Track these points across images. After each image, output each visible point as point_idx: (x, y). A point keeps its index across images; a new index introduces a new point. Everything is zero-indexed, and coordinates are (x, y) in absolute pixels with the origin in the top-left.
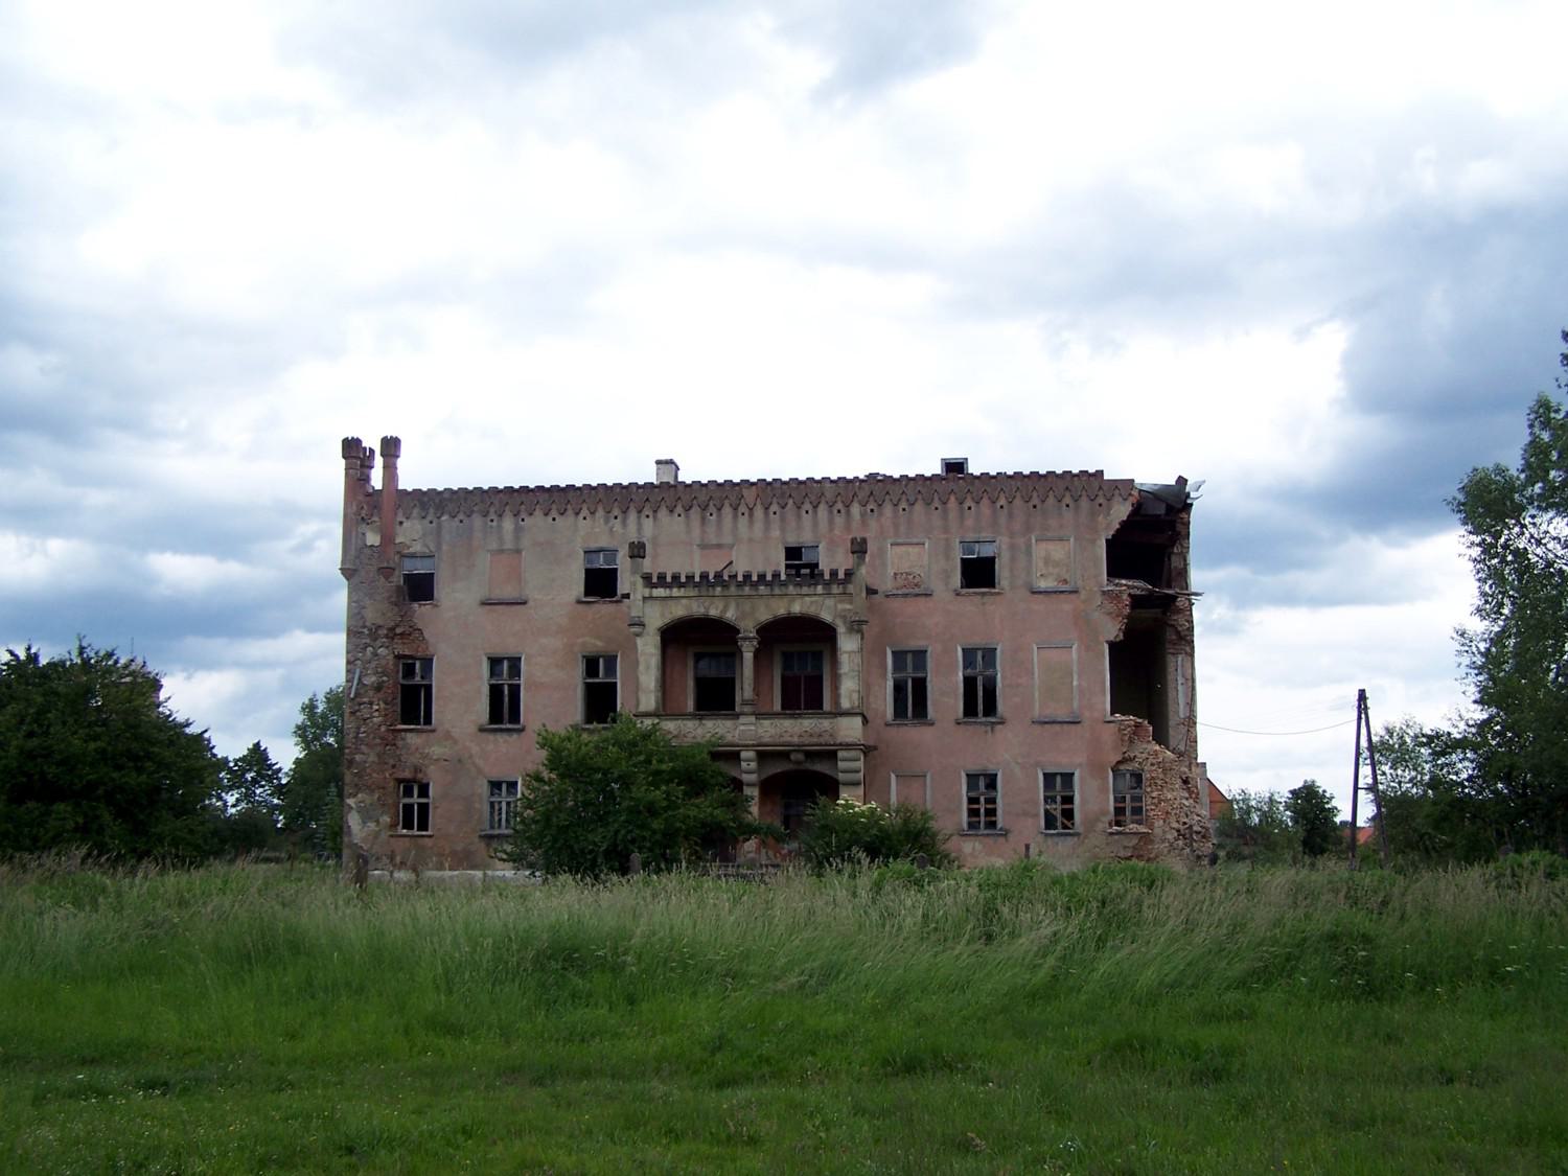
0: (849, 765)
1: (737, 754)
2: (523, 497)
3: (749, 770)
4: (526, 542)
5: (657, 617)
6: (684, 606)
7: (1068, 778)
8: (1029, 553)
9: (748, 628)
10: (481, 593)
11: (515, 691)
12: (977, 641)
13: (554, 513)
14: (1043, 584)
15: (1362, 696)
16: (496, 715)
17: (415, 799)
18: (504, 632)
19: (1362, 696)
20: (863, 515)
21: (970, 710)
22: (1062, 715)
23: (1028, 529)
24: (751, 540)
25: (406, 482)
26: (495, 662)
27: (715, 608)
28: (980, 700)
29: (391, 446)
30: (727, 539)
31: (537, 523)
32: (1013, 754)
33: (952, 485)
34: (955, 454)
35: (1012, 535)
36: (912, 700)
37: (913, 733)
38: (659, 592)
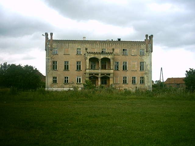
0: (111, 75)
1: (98, 74)
2: (124, 42)
3: (99, 76)
4: (69, 47)
5: (89, 57)
6: (92, 56)
7: (135, 78)
8: (131, 51)
9: (100, 59)
10: (63, 54)
11: (68, 66)
12: (125, 61)
13: (143, 45)
14: (132, 55)
15: (162, 68)
16: (65, 69)
17: (66, 79)
18: (66, 58)
19: (162, 68)
20: (111, 45)
21: (124, 69)
22: (134, 70)
23: (131, 48)
24: (98, 48)
25: (53, 39)
26: (65, 62)
27: (96, 56)
28: (125, 68)
29: (52, 34)
30: (95, 48)
31: (71, 45)
32: (129, 75)
33: (118, 42)
34: (119, 38)
35: (129, 48)
36: (117, 68)
37: (117, 72)
38: (89, 54)
